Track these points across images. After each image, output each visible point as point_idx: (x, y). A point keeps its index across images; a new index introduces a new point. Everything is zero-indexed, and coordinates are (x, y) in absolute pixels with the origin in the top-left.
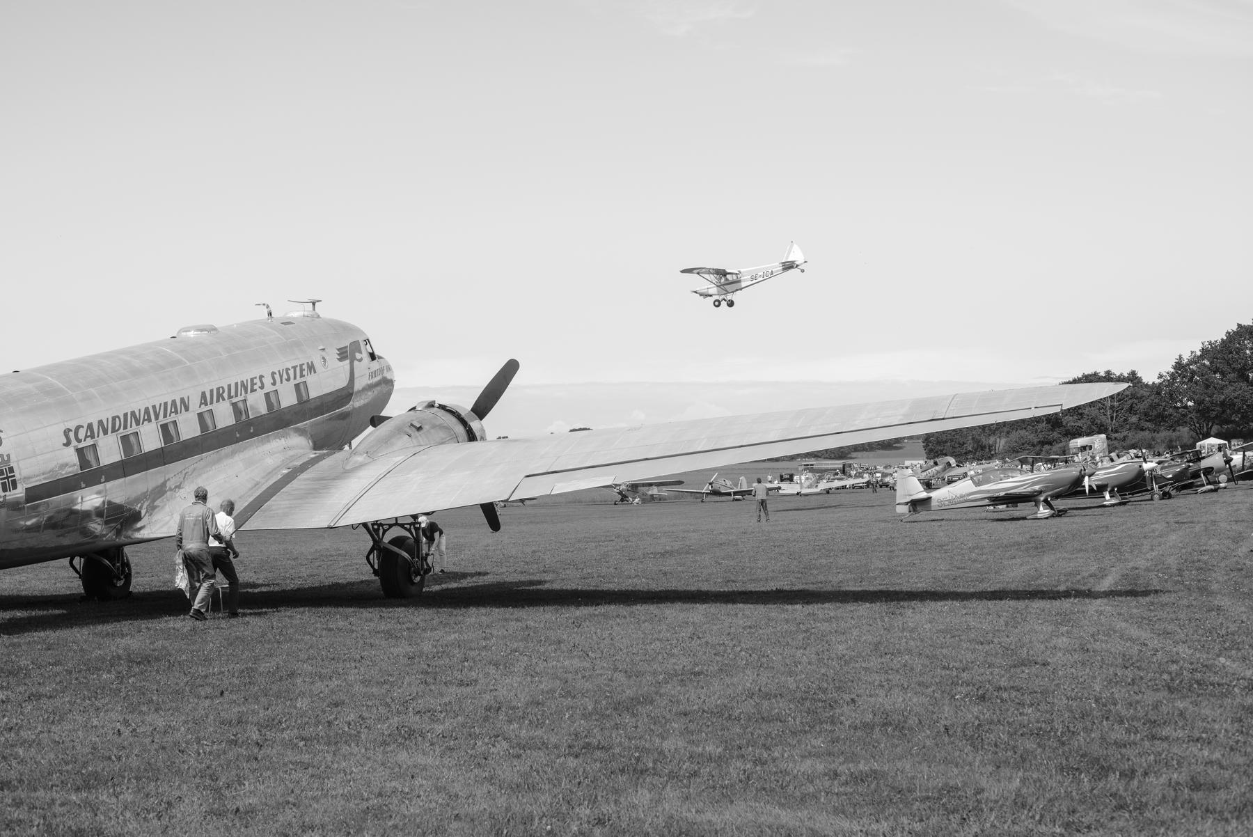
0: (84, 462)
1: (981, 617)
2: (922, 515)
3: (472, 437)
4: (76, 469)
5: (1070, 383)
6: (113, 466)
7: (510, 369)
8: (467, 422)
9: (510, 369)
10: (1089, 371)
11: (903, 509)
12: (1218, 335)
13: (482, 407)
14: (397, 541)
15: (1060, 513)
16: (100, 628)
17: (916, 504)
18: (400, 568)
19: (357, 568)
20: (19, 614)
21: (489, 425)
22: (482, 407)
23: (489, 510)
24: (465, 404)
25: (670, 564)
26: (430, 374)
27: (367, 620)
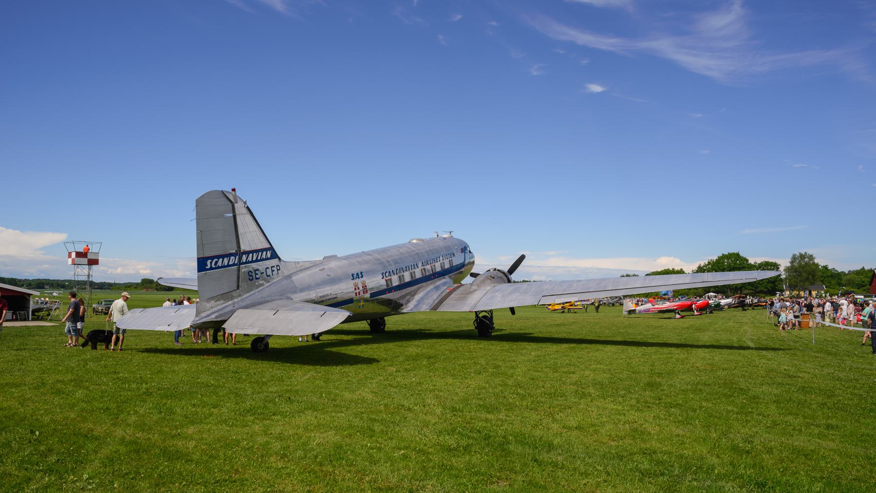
0: (387, 285)
1: (719, 356)
2: (633, 315)
3: (509, 281)
4: (385, 287)
5: (148, 351)
6: (420, 279)
7: (522, 257)
8: (506, 276)
9: (522, 257)
10: (655, 270)
11: (625, 313)
12: (715, 258)
13: (513, 269)
14: (484, 317)
15: (682, 317)
16: (397, 343)
17: (631, 312)
18: (484, 327)
19: (469, 325)
20: (359, 337)
21: (513, 277)
22: (513, 269)
23: (512, 310)
24: (506, 269)
25: (630, 331)
26: (484, 261)
27: (472, 344)
